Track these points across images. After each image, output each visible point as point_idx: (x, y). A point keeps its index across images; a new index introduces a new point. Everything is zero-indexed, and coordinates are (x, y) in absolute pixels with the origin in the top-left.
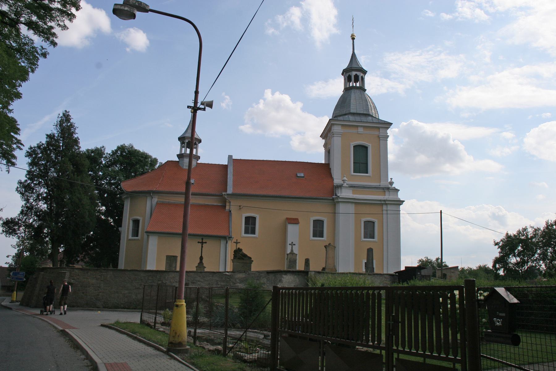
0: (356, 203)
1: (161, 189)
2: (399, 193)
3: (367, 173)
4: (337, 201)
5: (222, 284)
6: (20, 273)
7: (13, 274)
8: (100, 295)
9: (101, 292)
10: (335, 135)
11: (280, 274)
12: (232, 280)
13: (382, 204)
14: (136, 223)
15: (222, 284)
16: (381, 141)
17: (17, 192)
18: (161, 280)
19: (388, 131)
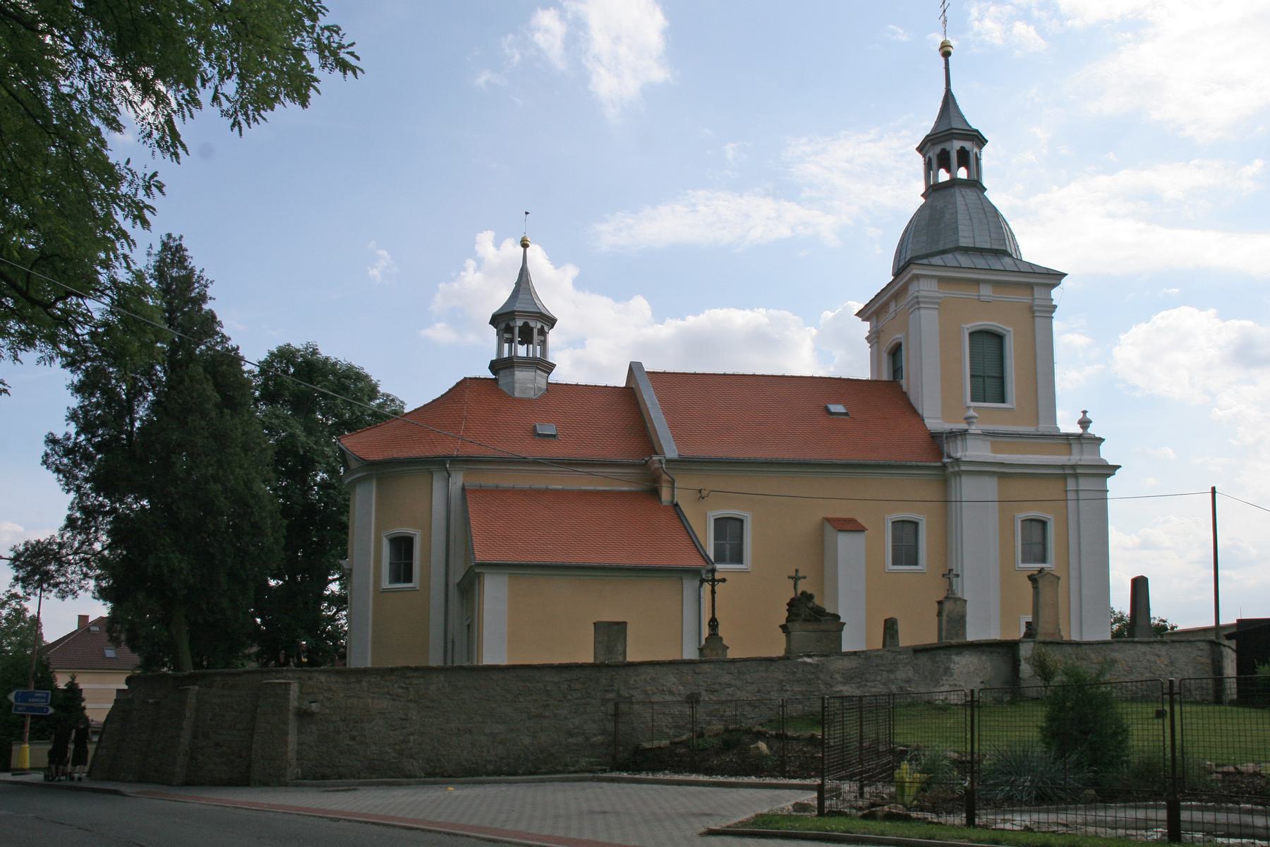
0: (1002, 476)
1: (473, 451)
2: (1103, 447)
3: (1003, 401)
4: (957, 472)
5: (797, 688)
6: (37, 695)
7: (16, 698)
8: (412, 740)
9: (412, 734)
10: (922, 306)
11: (945, 654)
12: (822, 676)
13: (1064, 477)
14: (402, 547)
15: (797, 688)
16: (1037, 319)
17: (45, 466)
18: (616, 688)
19: (1052, 291)
